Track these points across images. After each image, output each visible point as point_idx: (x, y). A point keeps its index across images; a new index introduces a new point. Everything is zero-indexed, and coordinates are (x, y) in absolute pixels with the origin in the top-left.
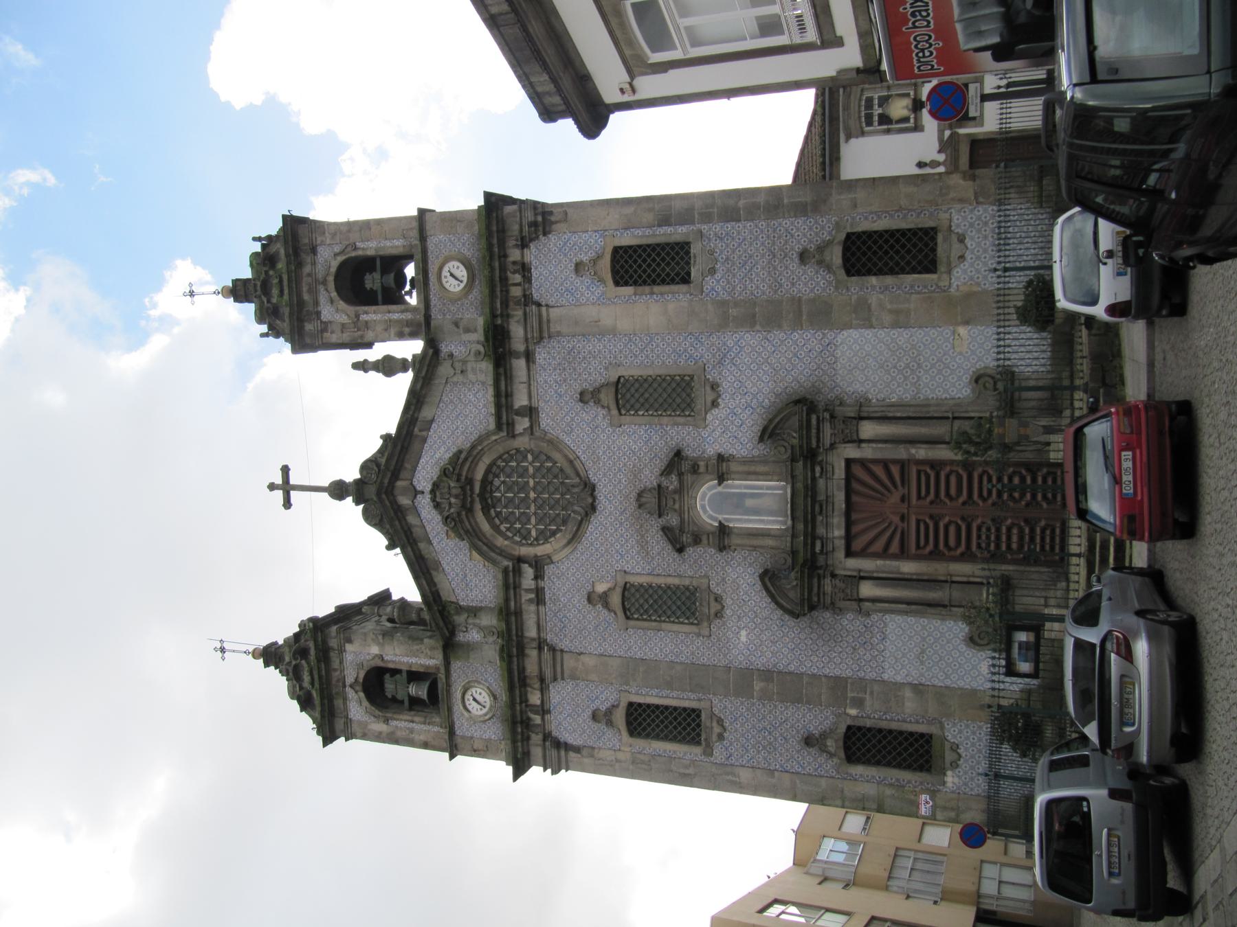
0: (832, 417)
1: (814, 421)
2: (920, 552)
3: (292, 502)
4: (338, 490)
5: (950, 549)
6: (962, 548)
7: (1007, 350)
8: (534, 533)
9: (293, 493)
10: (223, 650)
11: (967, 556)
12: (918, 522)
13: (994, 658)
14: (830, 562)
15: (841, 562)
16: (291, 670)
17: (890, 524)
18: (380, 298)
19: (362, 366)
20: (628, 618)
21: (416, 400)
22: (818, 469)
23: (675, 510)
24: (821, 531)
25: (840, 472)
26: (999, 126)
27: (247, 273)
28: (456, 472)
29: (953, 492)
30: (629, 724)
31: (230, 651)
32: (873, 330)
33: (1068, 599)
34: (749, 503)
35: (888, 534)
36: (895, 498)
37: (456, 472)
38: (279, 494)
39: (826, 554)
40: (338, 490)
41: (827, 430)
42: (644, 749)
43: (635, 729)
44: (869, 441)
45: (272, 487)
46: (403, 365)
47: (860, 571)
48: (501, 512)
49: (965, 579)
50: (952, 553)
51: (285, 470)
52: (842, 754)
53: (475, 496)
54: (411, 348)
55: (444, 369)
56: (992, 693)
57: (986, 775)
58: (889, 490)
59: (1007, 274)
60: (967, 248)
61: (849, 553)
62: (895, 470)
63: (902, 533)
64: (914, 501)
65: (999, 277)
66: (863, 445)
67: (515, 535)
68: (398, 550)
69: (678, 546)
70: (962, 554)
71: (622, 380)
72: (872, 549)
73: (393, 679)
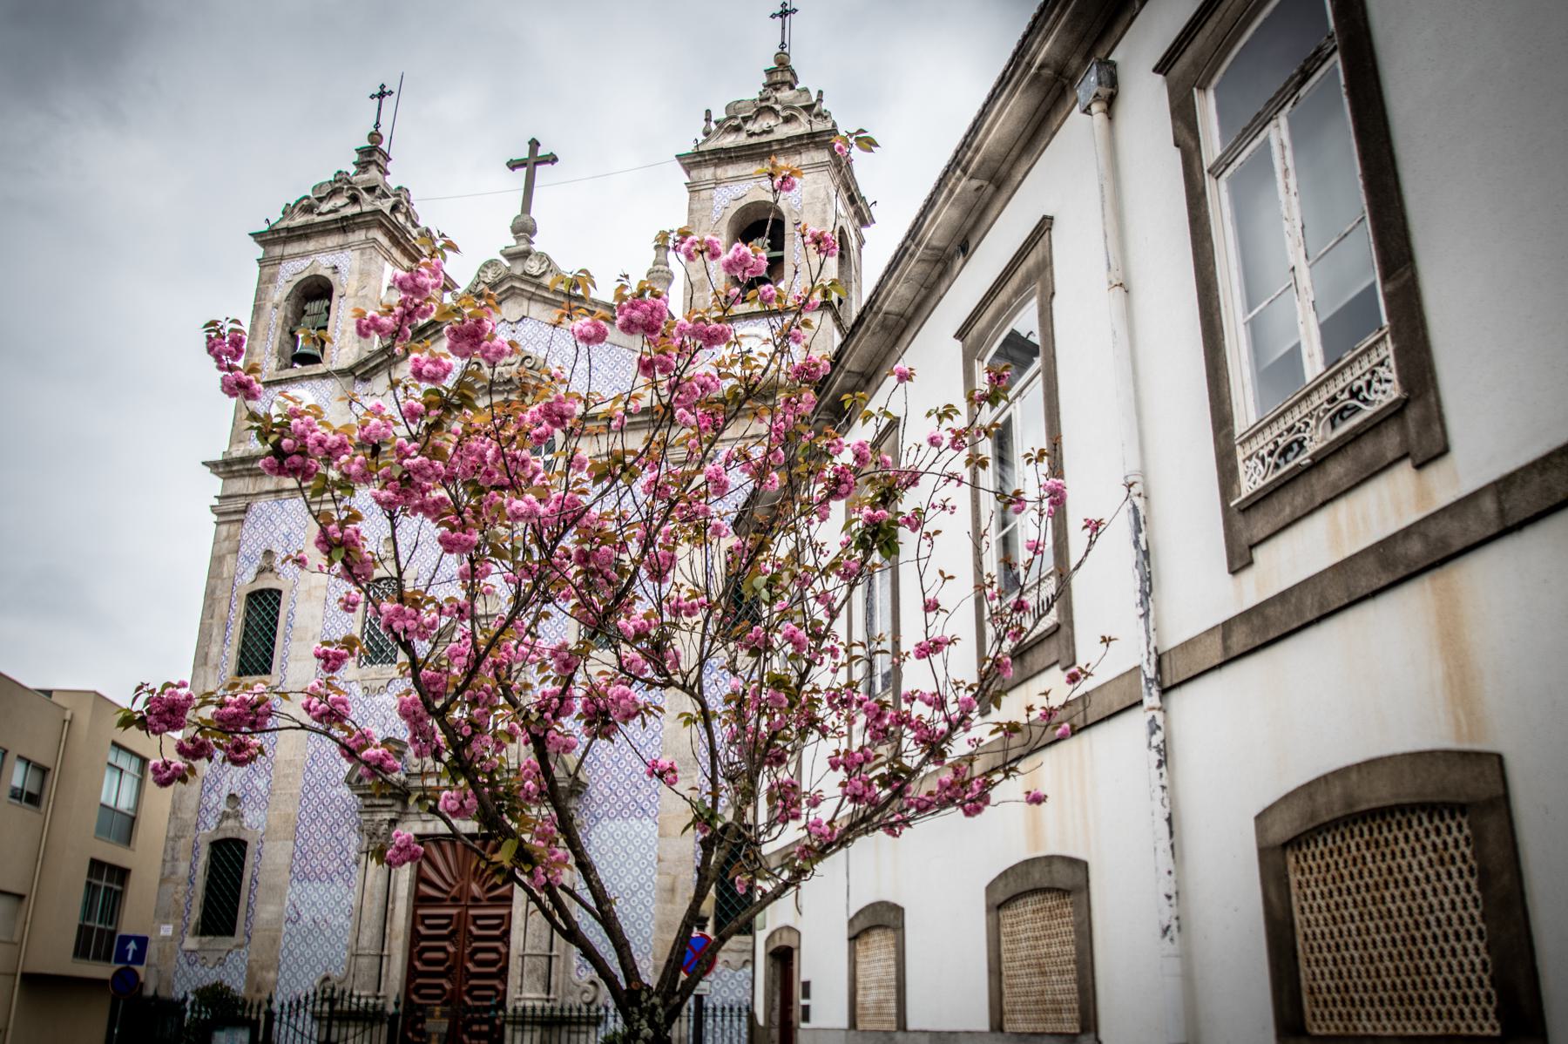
2: (419, 920)
10: (382, 95)
11: (411, 973)
14: (411, 817)
16: (768, 104)
17: (450, 885)
26: (710, 1005)
29: (480, 956)
30: (261, 592)
36: (475, 889)
43: (256, 599)
45: (534, 144)
51: (552, 159)
52: (220, 836)
60: (736, 970)
64: (472, 912)
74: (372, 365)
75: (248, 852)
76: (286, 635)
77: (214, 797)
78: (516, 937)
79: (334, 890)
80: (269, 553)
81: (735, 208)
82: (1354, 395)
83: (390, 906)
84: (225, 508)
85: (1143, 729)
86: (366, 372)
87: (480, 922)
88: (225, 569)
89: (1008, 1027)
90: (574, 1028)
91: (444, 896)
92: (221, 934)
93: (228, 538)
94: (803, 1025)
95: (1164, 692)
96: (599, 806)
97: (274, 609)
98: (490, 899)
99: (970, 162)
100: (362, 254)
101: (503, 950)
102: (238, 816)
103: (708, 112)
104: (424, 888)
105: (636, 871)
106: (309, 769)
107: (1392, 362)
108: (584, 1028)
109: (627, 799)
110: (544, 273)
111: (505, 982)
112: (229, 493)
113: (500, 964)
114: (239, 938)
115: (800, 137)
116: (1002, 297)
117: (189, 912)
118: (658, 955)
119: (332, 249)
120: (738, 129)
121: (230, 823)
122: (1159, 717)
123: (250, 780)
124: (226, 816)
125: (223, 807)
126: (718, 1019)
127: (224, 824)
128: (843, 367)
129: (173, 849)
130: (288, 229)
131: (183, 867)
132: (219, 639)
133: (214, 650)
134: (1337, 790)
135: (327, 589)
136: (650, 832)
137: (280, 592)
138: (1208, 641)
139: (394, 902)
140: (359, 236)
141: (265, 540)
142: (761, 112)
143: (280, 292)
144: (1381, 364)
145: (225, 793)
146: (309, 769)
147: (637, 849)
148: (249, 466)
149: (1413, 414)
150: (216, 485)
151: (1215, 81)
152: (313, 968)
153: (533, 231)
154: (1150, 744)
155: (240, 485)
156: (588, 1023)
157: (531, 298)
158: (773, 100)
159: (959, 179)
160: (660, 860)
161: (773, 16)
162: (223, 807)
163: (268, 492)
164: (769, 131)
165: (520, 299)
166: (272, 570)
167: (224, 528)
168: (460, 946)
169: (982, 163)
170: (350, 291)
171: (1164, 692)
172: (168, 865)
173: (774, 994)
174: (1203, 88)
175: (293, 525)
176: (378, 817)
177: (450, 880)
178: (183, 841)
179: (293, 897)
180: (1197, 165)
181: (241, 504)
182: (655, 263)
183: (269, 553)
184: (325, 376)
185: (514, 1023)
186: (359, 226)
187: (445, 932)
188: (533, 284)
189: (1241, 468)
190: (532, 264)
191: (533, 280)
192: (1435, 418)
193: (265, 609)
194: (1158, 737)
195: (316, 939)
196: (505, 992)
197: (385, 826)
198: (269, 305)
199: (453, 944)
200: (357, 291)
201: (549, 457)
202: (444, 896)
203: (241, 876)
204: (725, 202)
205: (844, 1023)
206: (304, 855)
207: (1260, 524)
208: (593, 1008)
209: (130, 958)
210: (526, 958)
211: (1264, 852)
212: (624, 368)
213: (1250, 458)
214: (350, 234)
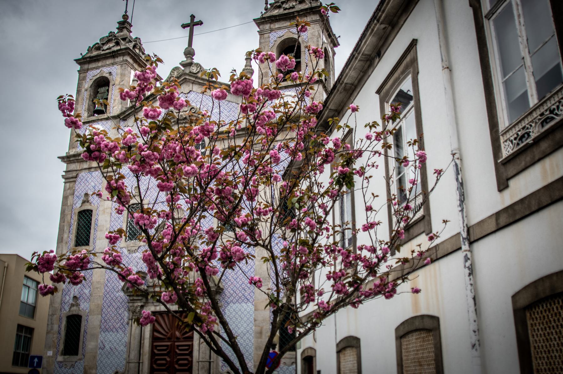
3: (186, 28)
32: (253, 321)
36: (177, 333)
42: (73, 219)
45: (193, 17)
49: (140, 369)
52: (71, 314)
53: (184, 124)
64: (176, 344)
74: (127, 113)
76: (95, 229)
77: (68, 298)
81: (279, 41)
82: (552, 112)
86: (125, 117)
87: (180, 348)
88: (69, 202)
96: (229, 298)
98: (184, 338)
100: (121, 67)
102: (78, 305)
104: (156, 334)
105: (245, 325)
106: (106, 285)
109: (240, 295)
110: (198, 72)
112: (69, 170)
114: (80, 356)
116: (396, 75)
117: (59, 345)
119: (109, 65)
121: (74, 308)
123: (82, 290)
124: (72, 305)
129: (51, 320)
130: (90, 57)
131: (56, 327)
132: (67, 231)
136: (251, 309)
137: (92, 211)
140: (120, 59)
143: (87, 84)
145: (72, 296)
150: (64, 166)
152: (111, 368)
153: (193, 54)
154: (465, 266)
155: (73, 166)
157: (193, 83)
159: (376, 25)
160: (255, 320)
163: (85, 169)
166: (88, 202)
170: (117, 83)
171: (471, 243)
172: (50, 326)
176: (136, 305)
178: (55, 316)
179: (102, 338)
181: (74, 174)
182: (246, 66)
183: (86, 195)
184: (107, 119)
186: (120, 55)
187: (165, 352)
188: (194, 77)
189: (502, 146)
190: (193, 68)
193: (86, 218)
195: (111, 356)
197: (139, 308)
198: (83, 90)
199: (169, 357)
200: (120, 82)
206: (106, 321)
207: (511, 170)
210: (200, 363)
212: (234, 111)
213: (506, 141)
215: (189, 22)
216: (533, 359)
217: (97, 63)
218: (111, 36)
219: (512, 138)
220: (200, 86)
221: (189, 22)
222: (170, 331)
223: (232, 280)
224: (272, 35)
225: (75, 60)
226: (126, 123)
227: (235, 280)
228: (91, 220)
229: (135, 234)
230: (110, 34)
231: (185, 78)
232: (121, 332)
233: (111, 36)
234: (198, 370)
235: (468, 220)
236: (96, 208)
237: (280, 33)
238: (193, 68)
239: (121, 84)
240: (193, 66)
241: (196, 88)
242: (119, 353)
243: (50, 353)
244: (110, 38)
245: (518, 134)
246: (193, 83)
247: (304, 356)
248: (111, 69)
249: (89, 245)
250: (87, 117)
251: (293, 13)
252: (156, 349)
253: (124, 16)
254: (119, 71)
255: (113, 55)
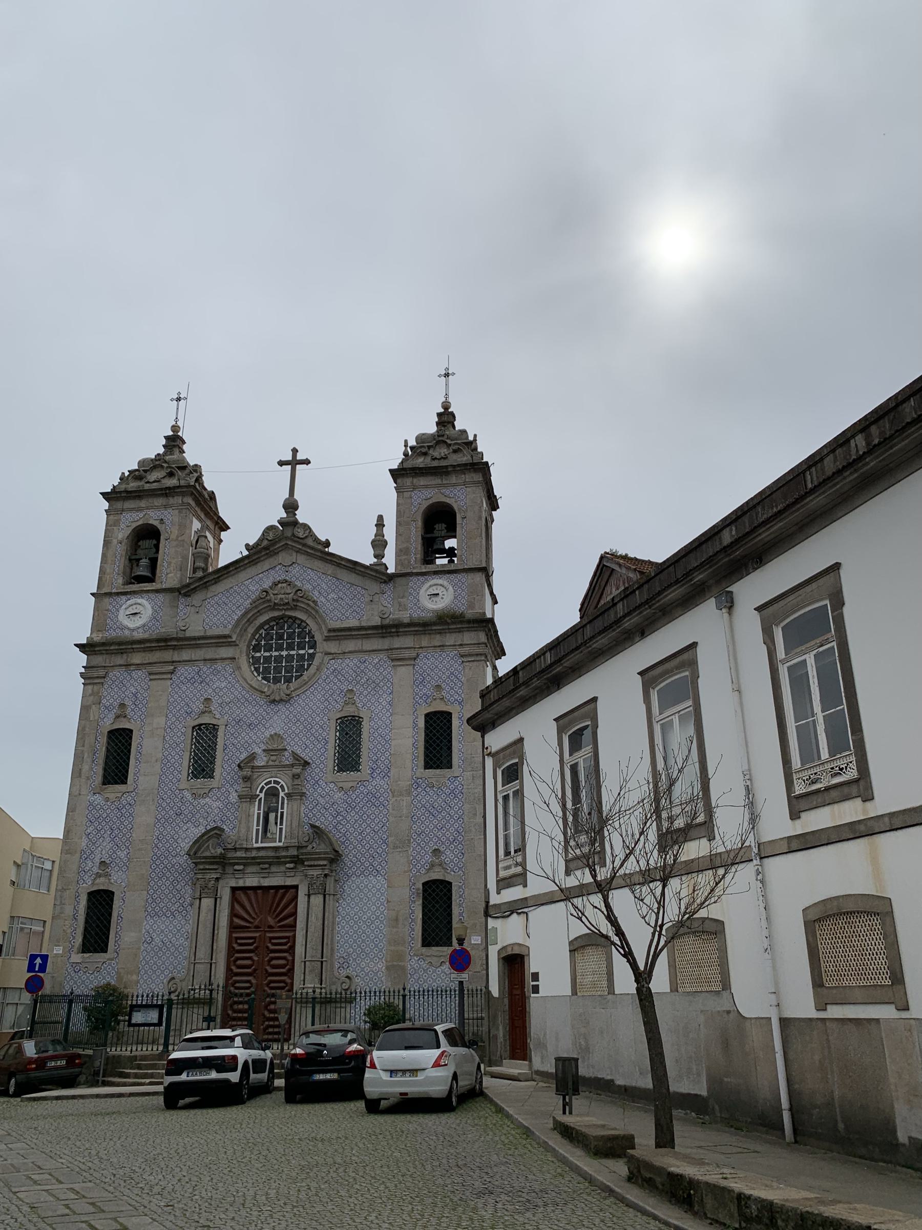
0: (326, 875)
1: (322, 863)
2: (234, 941)
4: (291, 506)
5: (235, 961)
6: (235, 970)
7: (368, 998)
8: (258, 655)
9: (290, 467)
10: (179, 399)
11: (229, 973)
12: (254, 938)
13: (163, 996)
15: (227, 884)
17: (253, 918)
18: (428, 536)
19: (380, 524)
20: (193, 728)
21: (353, 566)
22: (292, 865)
23: (268, 762)
24: (250, 869)
25: (289, 882)
27: (459, 425)
28: (300, 599)
29: (274, 962)
31: (178, 405)
33: (142, 1044)
34: (272, 816)
35: (246, 916)
36: (271, 921)
37: (300, 599)
38: (289, 457)
39: (233, 874)
40: (291, 506)
41: (315, 872)
44: (309, 902)
45: (295, 451)
46: (379, 556)
47: (221, 898)
48: (273, 630)
50: (232, 963)
51: (307, 462)
53: (283, 612)
54: (390, 561)
55: (374, 587)
56: (135, 994)
57: (72, 993)
58: (277, 916)
59: (401, 997)
61: (234, 890)
62: (289, 921)
63: (249, 927)
64: (268, 935)
65: (399, 992)
66: (307, 897)
67: (256, 641)
68: (246, 553)
69: (242, 765)
70: (231, 970)
71: (361, 720)
72: (237, 907)
73: (152, 546)
74: (192, 587)
75: (115, 898)
76: (137, 759)
77: (90, 864)
78: (299, 949)
79: (175, 922)
80: (122, 706)
81: (425, 505)
82: (841, 769)
83: (216, 932)
84: (90, 675)
85: (754, 874)
86: (188, 591)
87: (273, 941)
88: (92, 715)
89: (680, 990)
90: (339, 1005)
91: (250, 925)
92: (96, 951)
93: (92, 694)
94: (533, 995)
95: (761, 858)
96: (350, 868)
97: (127, 741)
98: (280, 927)
99: (654, 604)
100: (180, 512)
101: (290, 958)
102: (107, 875)
103: (406, 441)
104: (236, 920)
105: (373, 908)
106: (156, 846)
107: (854, 762)
108: (343, 1005)
109: (367, 864)
110: (306, 537)
111: (292, 978)
112: (92, 664)
113: (288, 967)
114: (110, 953)
115: (466, 465)
116: (667, 666)
117: (74, 938)
118: (388, 960)
119: (158, 507)
120: (425, 454)
121: (102, 880)
122: (760, 868)
123: (114, 852)
124: (98, 875)
125: (96, 870)
126: (426, 997)
127: (98, 881)
128: (562, 664)
129: (61, 897)
130: (126, 491)
131: (69, 910)
132: (89, 760)
133: (86, 767)
134: (835, 903)
135: (165, 730)
136: (382, 884)
137: (131, 731)
138: (782, 842)
139: (218, 930)
140: (178, 500)
141: (119, 696)
142: (438, 443)
143: (123, 533)
144: (851, 762)
145: (97, 861)
146: (156, 846)
147: (374, 895)
148: (108, 648)
149: (862, 783)
150: (83, 659)
151: (782, 624)
152: (162, 972)
153: (296, 508)
154: (757, 880)
155: (98, 660)
156: (346, 1002)
157: (298, 551)
158: (446, 436)
159: (646, 609)
160: (388, 902)
161: (440, 376)
162: (96, 870)
163: (120, 665)
164: (445, 458)
165: (291, 551)
166: (125, 717)
167: (90, 687)
168: (261, 956)
169: (660, 605)
170: (173, 536)
171: (761, 858)
172: (58, 908)
173: (504, 980)
174: (777, 625)
175: (139, 688)
176: (208, 876)
177: (254, 915)
178: (68, 892)
179: (148, 927)
180: (775, 658)
181: (102, 672)
182: (376, 536)
183: (122, 706)
184: (157, 591)
185: (321, 1003)
186: (178, 494)
187: (251, 947)
188: (300, 544)
189: (795, 782)
190: (299, 530)
191: (301, 541)
192: (869, 787)
193: (120, 742)
194: (760, 877)
195: (164, 954)
196: (292, 984)
197: (213, 882)
198: (115, 541)
199: (257, 955)
200: (178, 537)
201: (311, 651)
202: (250, 925)
203: (110, 915)
204: (419, 501)
205: (569, 992)
206: (154, 901)
207: (803, 804)
208: (348, 993)
209: (37, 969)
210: (307, 963)
211: (806, 924)
212: (359, 600)
213: (799, 779)
214: (171, 499)
215: (291, 459)
216: (822, 962)
217: (138, 502)
218: (159, 460)
219: (805, 778)
220: (308, 557)
221: (291, 459)
222: (258, 916)
223: (355, 843)
224: (416, 494)
225: (101, 493)
226: (189, 599)
227: (360, 842)
228: (130, 745)
229: (203, 770)
230: (157, 458)
231: (286, 544)
232: (179, 918)
233: (159, 460)
234: (304, 973)
235: (759, 839)
236: (140, 726)
237: (428, 493)
238: (299, 530)
239: (180, 539)
240: (298, 528)
241: (301, 559)
242: (177, 949)
243: (58, 950)
244: (157, 463)
245: (810, 778)
246: (297, 552)
247: (503, 956)
248: (162, 513)
249: (126, 783)
250: (124, 585)
251: (446, 467)
252: (236, 943)
253: (173, 426)
254: (176, 519)
255: (166, 493)
